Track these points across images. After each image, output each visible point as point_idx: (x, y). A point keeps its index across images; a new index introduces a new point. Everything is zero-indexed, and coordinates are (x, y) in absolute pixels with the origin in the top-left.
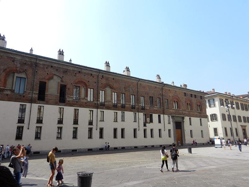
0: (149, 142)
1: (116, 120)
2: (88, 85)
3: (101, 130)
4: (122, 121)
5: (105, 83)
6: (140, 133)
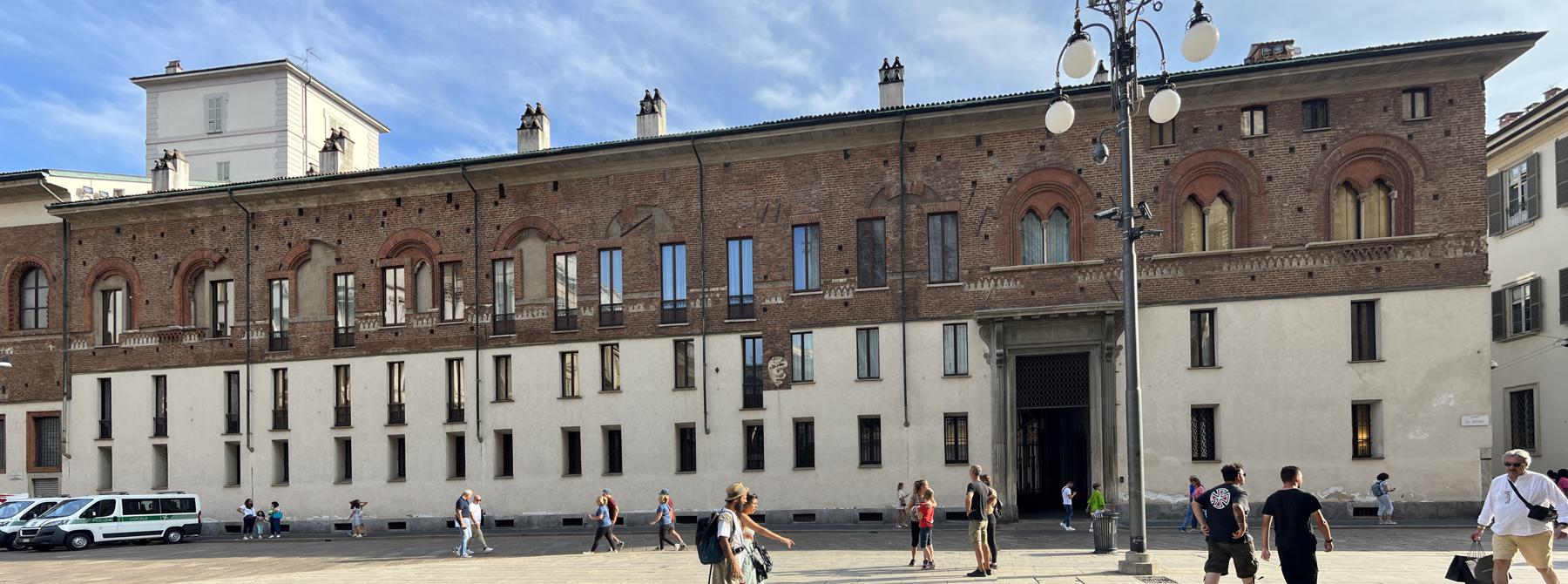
0: (586, 493)
1: (568, 393)
2: (436, 250)
3: (505, 440)
4: (564, 396)
5: (513, 219)
6: (721, 448)
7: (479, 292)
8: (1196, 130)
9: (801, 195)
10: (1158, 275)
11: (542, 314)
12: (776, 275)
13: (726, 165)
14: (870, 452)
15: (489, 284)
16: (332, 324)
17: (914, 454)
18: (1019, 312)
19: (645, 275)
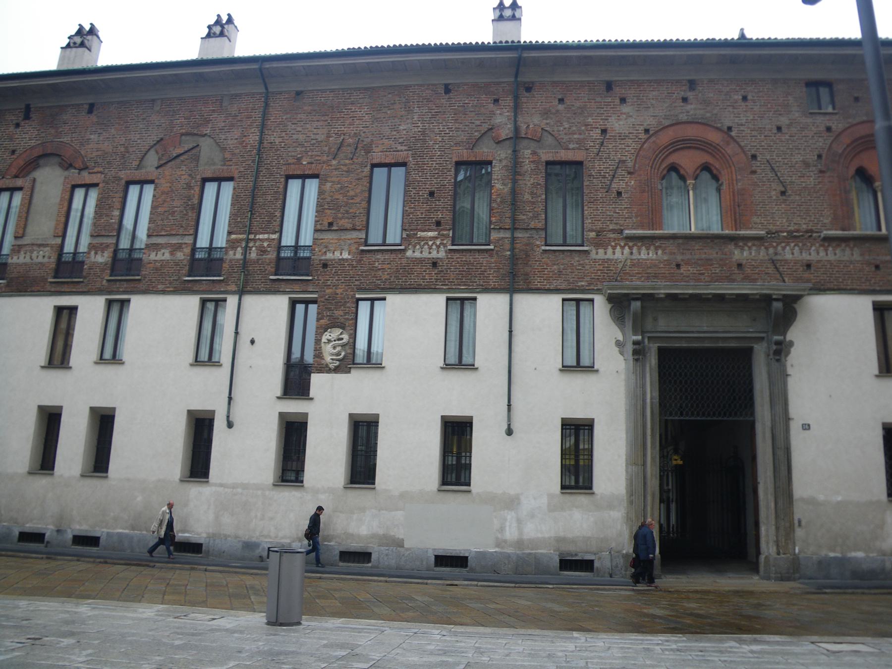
1: (59, 356)
5: (33, 143)
6: (246, 451)
8: (857, 99)
9: (386, 130)
10: (831, 257)
11: (45, 257)
12: (345, 223)
13: (298, 93)
14: (456, 466)
17: (517, 467)
18: (663, 289)
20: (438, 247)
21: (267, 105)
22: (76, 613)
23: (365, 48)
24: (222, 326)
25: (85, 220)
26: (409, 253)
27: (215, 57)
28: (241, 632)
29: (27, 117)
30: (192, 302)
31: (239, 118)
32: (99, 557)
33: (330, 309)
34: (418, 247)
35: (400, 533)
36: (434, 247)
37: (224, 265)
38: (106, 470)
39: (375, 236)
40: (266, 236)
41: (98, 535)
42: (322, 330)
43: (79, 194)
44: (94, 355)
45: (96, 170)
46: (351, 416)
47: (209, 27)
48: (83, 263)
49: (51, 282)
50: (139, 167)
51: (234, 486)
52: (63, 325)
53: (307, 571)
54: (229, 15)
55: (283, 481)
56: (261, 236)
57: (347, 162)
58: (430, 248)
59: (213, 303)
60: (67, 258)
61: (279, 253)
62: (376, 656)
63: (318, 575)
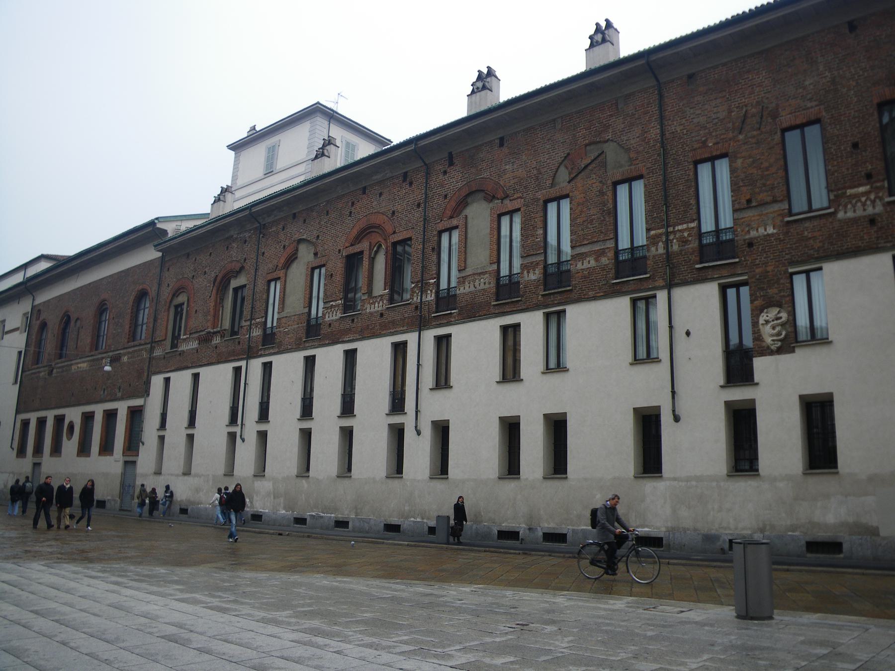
1: (511, 372)
3: (442, 430)
5: (460, 185)
6: (697, 442)
7: (424, 268)
11: (485, 284)
12: (765, 196)
13: (690, 77)
15: (435, 258)
16: (305, 317)
19: (598, 221)
20: (873, 202)
21: (661, 96)
22: (554, 603)
23: (750, 10)
24: (656, 323)
25: (514, 244)
26: (841, 215)
27: (602, 63)
28: (712, 625)
29: (451, 164)
30: (624, 303)
31: (636, 116)
32: (567, 553)
33: (762, 289)
34: (849, 206)
35: (873, 520)
36: (868, 203)
37: (648, 262)
38: (565, 471)
39: (799, 203)
40: (685, 226)
41: (564, 532)
42: (757, 312)
43: (505, 221)
44: (541, 367)
45: (515, 196)
46: (802, 398)
47: (591, 37)
48: (518, 283)
49: (494, 305)
50: (553, 185)
51: (688, 479)
52: (510, 342)
53: (774, 563)
54: (607, 20)
55: (737, 471)
56: (680, 227)
57: (755, 133)
58: (864, 204)
59: (644, 302)
60: (505, 281)
61: (700, 240)
62: (863, 656)
63: (786, 567)
